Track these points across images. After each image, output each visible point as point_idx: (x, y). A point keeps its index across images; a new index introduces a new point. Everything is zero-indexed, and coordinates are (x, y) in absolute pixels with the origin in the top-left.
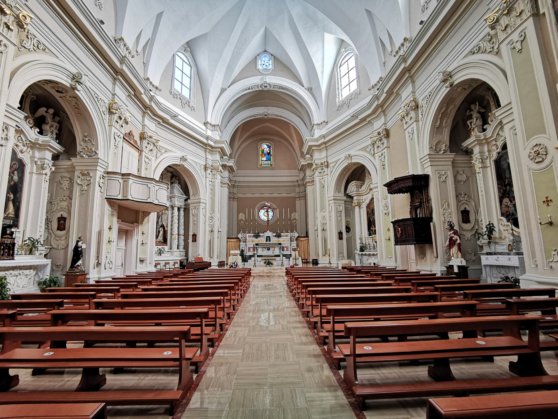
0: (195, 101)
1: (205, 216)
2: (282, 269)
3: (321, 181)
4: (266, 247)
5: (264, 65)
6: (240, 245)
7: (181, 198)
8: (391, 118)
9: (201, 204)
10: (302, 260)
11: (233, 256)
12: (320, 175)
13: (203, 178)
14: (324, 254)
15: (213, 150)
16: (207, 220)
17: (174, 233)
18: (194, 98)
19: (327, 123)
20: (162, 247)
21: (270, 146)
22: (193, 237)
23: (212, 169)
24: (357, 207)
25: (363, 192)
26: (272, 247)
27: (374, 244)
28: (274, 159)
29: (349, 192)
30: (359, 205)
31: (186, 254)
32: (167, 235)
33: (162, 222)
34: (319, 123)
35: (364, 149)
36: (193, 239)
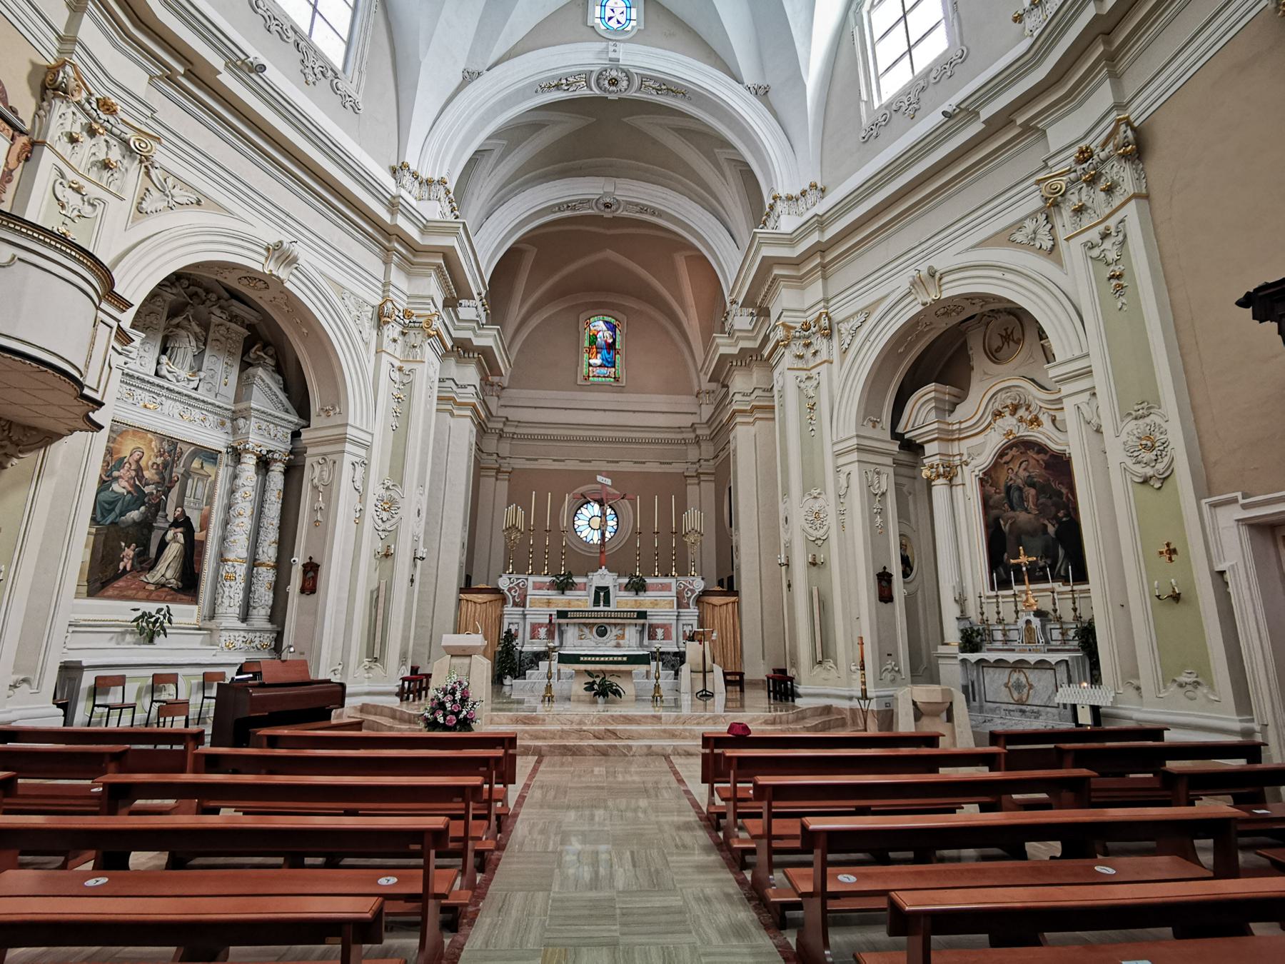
0: (363, 85)
1: (362, 496)
2: (658, 719)
3: (802, 385)
4: (594, 624)
5: (610, 19)
6: (501, 616)
7: (277, 421)
8: (1155, 71)
9: (348, 447)
10: (725, 674)
11: (455, 660)
12: (800, 364)
13: (368, 350)
14: (819, 658)
15: (416, 260)
16: (370, 510)
17: (231, 556)
18: (360, 72)
19: (823, 191)
20: (164, 606)
21: (615, 327)
22: (305, 572)
23: (404, 326)
24: (942, 481)
25: (963, 426)
26: (615, 625)
27: (1028, 622)
28: (627, 364)
29: (909, 428)
30: (949, 474)
31: (276, 640)
32: (201, 563)
33: (180, 504)
34: (796, 192)
35: (1006, 238)
36: (304, 581)
